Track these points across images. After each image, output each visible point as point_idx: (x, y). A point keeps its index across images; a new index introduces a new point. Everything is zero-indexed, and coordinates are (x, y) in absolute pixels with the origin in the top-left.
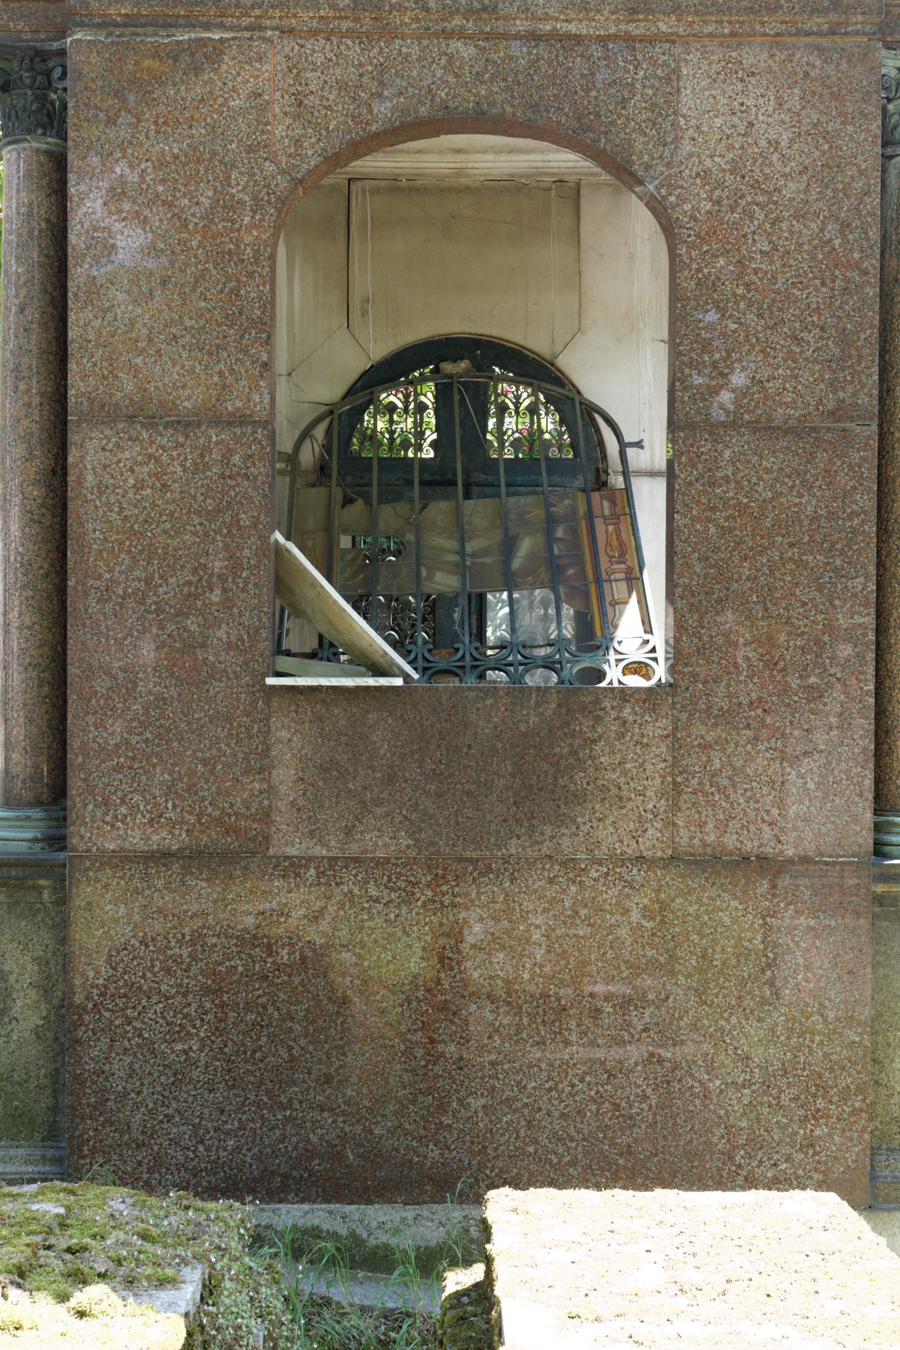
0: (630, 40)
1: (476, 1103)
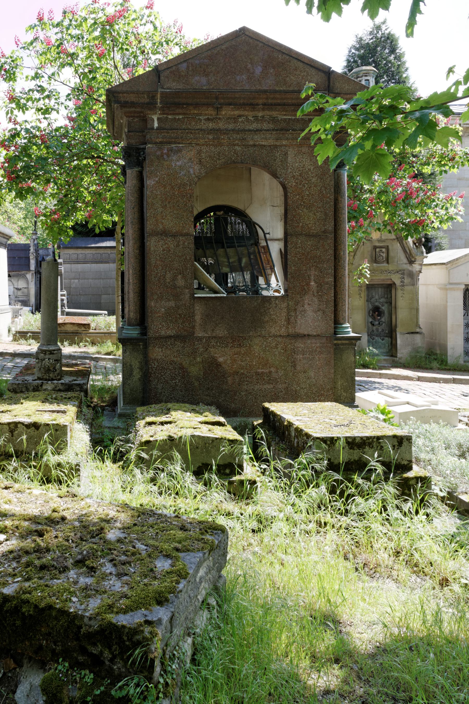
0: (276, 146)
1: (243, 393)
